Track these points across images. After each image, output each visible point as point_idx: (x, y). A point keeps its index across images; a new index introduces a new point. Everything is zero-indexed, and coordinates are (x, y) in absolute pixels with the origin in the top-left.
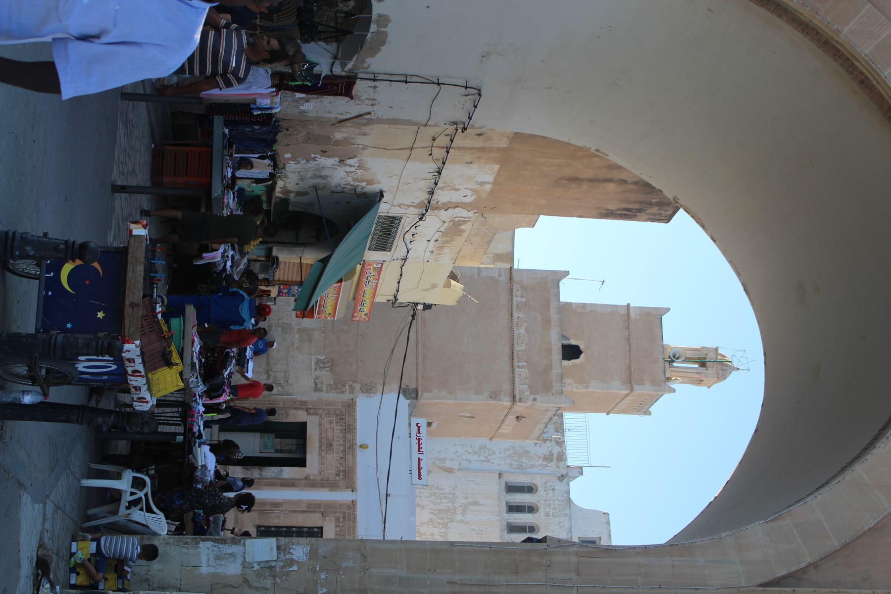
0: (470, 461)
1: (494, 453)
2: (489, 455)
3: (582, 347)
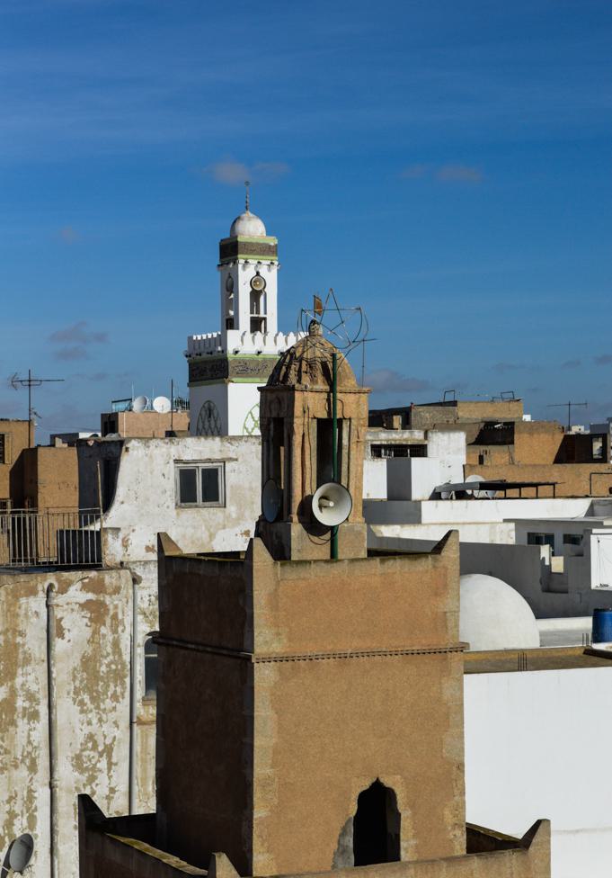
0: (112, 790)
1: (91, 737)
2: (95, 747)
3: (366, 784)
